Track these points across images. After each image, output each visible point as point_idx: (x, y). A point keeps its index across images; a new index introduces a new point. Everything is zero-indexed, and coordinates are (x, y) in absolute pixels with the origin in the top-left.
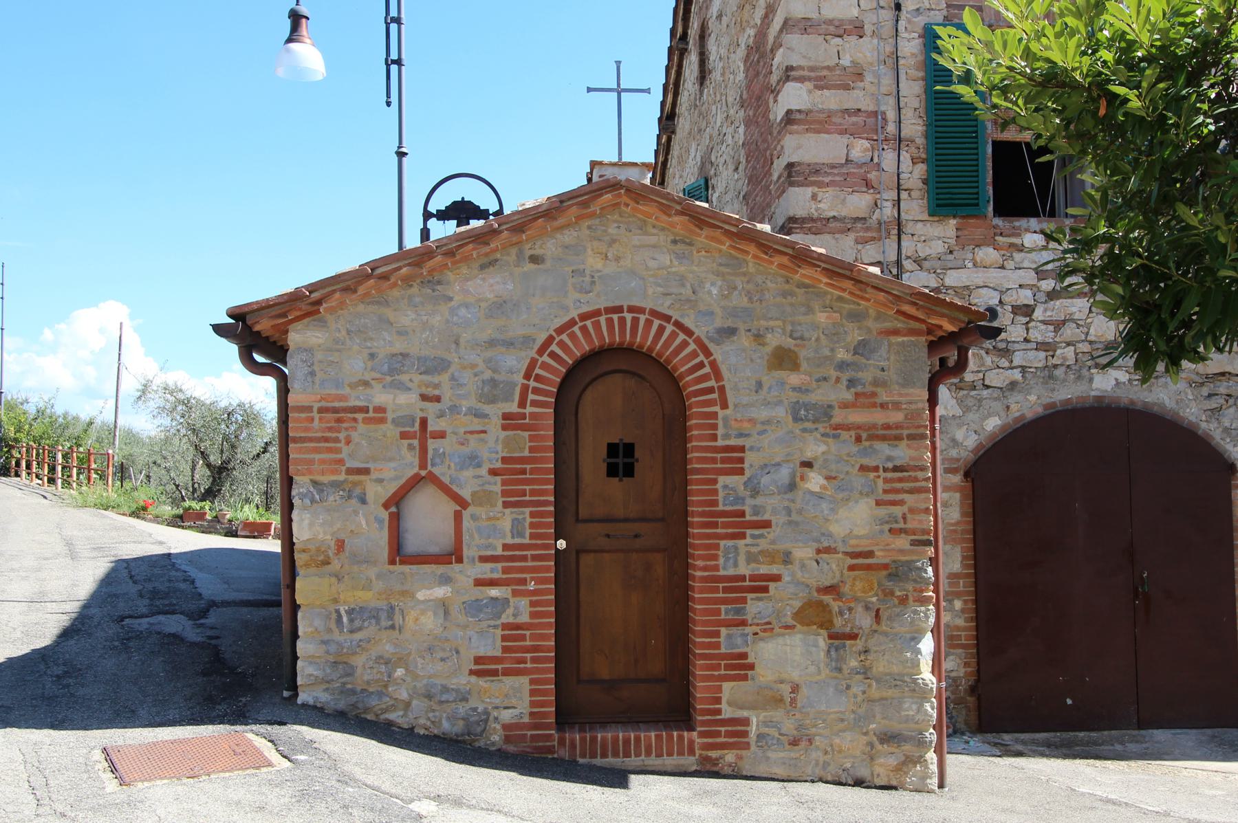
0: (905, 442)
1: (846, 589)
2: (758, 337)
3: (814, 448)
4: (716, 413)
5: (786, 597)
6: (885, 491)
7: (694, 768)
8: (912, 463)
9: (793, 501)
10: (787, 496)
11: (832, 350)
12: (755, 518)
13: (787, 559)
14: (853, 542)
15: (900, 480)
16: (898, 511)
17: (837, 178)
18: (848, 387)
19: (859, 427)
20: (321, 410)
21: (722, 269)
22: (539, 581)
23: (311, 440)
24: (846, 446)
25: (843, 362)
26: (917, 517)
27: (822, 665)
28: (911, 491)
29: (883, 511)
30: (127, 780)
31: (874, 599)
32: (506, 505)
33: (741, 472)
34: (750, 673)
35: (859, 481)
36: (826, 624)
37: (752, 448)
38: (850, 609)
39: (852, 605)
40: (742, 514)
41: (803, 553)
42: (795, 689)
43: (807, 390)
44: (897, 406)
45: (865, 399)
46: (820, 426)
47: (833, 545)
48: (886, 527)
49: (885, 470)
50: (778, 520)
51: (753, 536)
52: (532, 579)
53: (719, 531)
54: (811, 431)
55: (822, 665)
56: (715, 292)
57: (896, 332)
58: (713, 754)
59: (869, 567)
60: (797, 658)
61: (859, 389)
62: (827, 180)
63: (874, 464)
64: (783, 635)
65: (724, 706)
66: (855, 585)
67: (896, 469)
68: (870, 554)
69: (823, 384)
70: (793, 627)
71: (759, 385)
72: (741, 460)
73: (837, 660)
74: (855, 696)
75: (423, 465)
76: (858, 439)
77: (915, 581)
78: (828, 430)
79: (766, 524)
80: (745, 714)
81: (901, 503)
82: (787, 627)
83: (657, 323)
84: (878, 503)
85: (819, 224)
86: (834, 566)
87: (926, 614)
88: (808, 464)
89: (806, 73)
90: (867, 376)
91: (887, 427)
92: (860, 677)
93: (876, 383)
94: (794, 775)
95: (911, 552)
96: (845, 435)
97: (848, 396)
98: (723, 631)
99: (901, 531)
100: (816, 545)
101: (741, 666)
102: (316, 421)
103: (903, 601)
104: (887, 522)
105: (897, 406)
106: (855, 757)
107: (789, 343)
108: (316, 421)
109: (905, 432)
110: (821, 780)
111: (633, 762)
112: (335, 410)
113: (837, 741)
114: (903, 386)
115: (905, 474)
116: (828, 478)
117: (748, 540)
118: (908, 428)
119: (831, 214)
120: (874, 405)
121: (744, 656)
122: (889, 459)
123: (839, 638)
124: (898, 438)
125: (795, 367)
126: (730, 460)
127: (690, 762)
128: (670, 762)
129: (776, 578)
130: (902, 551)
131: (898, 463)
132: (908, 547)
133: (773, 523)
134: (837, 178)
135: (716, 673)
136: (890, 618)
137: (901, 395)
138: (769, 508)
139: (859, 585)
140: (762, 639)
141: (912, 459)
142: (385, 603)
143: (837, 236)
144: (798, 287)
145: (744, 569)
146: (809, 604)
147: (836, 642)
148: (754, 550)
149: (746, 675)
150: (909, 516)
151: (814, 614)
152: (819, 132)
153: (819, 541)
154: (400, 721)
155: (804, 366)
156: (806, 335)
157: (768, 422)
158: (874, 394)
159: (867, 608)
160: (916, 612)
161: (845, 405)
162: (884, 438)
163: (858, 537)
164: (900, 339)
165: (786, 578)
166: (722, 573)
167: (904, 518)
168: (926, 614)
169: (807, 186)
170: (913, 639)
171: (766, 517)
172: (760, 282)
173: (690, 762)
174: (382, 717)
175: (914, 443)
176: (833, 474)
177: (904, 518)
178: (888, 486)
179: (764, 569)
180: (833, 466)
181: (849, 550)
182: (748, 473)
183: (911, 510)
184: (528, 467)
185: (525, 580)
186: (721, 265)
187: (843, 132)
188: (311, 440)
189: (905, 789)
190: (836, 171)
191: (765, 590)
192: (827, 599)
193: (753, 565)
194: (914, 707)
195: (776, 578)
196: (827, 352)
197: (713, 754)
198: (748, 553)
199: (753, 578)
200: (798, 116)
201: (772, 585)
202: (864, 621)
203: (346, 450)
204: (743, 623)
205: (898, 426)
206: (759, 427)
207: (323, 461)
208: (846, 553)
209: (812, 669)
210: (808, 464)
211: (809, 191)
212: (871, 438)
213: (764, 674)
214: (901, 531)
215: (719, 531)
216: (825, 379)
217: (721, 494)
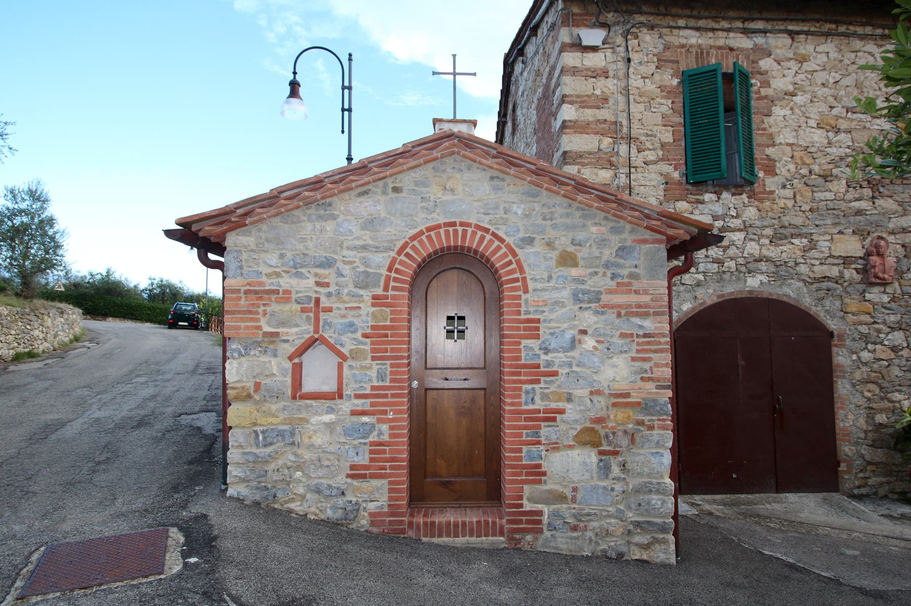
3: (589, 319)
6: (638, 351)
15: (649, 343)
16: (647, 365)
19: (620, 306)
28: (655, 351)
33: (537, 337)
34: (543, 478)
45: (623, 287)
49: (638, 336)
54: (587, 309)
57: (644, 241)
61: (620, 280)
66: (617, 416)
68: (627, 395)
72: (538, 329)
80: (540, 507)
88: (584, 332)
91: (639, 306)
93: (632, 276)
97: (612, 284)
99: (649, 379)
101: (536, 473)
104: (639, 373)
105: (646, 292)
109: (652, 311)
115: (653, 339)
117: (542, 385)
120: (630, 292)
129: (562, 412)
145: (539, 404)
151: (589, 437)
158: (630, 284)
161: (610, 292)
162: (637, 314)
182: (542, 339)
187: (596, 133)
191: (554, 419)
195: (562, 412)
200: (569, 124)
204: (539, 443)
205: (647, 306)
210: (584, 332)
214: (649, 379)
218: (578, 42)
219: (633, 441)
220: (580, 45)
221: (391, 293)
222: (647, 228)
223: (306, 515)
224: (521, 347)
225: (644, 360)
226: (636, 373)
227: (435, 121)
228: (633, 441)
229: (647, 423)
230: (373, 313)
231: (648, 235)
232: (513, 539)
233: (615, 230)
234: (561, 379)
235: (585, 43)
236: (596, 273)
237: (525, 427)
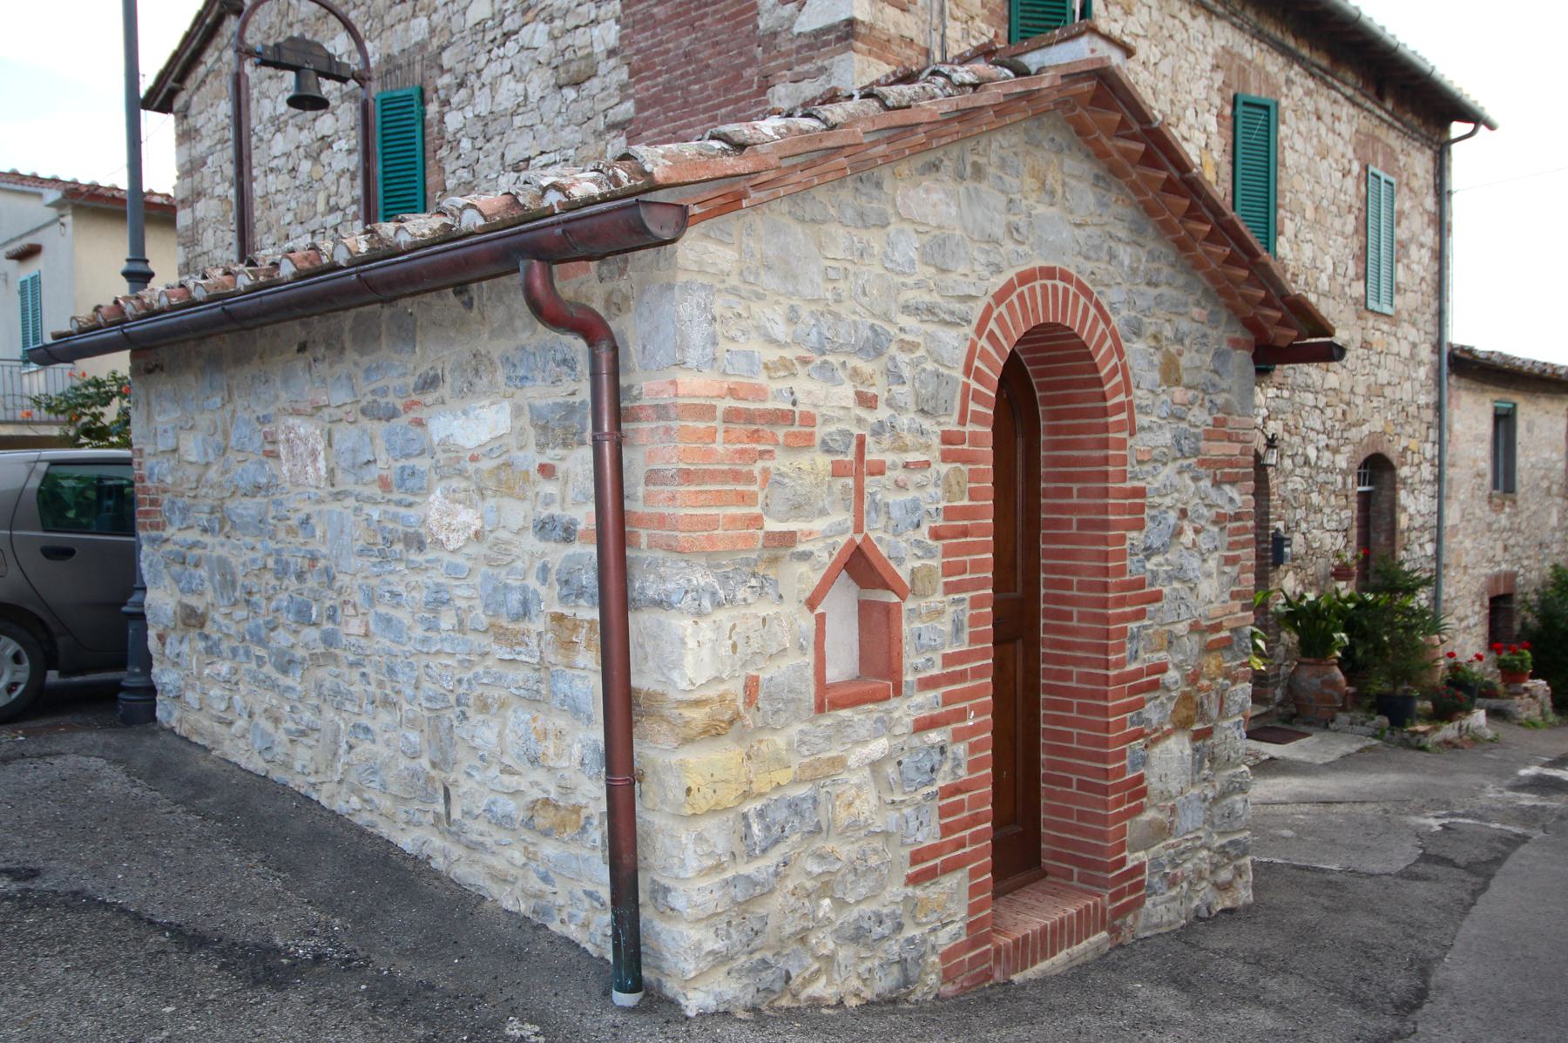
4: (1160, 592)
20: (732, 416)
23: (713, 476)
30: (1446, 943)
52: (972, 707)
75: (858, 528)
102: (720, 437)
108: (720, 437)
112: (750, 417)
149: (946, 519)
174: (803, 995)
188: (713, 476)
207: (733, 520)
221: (970, 428)
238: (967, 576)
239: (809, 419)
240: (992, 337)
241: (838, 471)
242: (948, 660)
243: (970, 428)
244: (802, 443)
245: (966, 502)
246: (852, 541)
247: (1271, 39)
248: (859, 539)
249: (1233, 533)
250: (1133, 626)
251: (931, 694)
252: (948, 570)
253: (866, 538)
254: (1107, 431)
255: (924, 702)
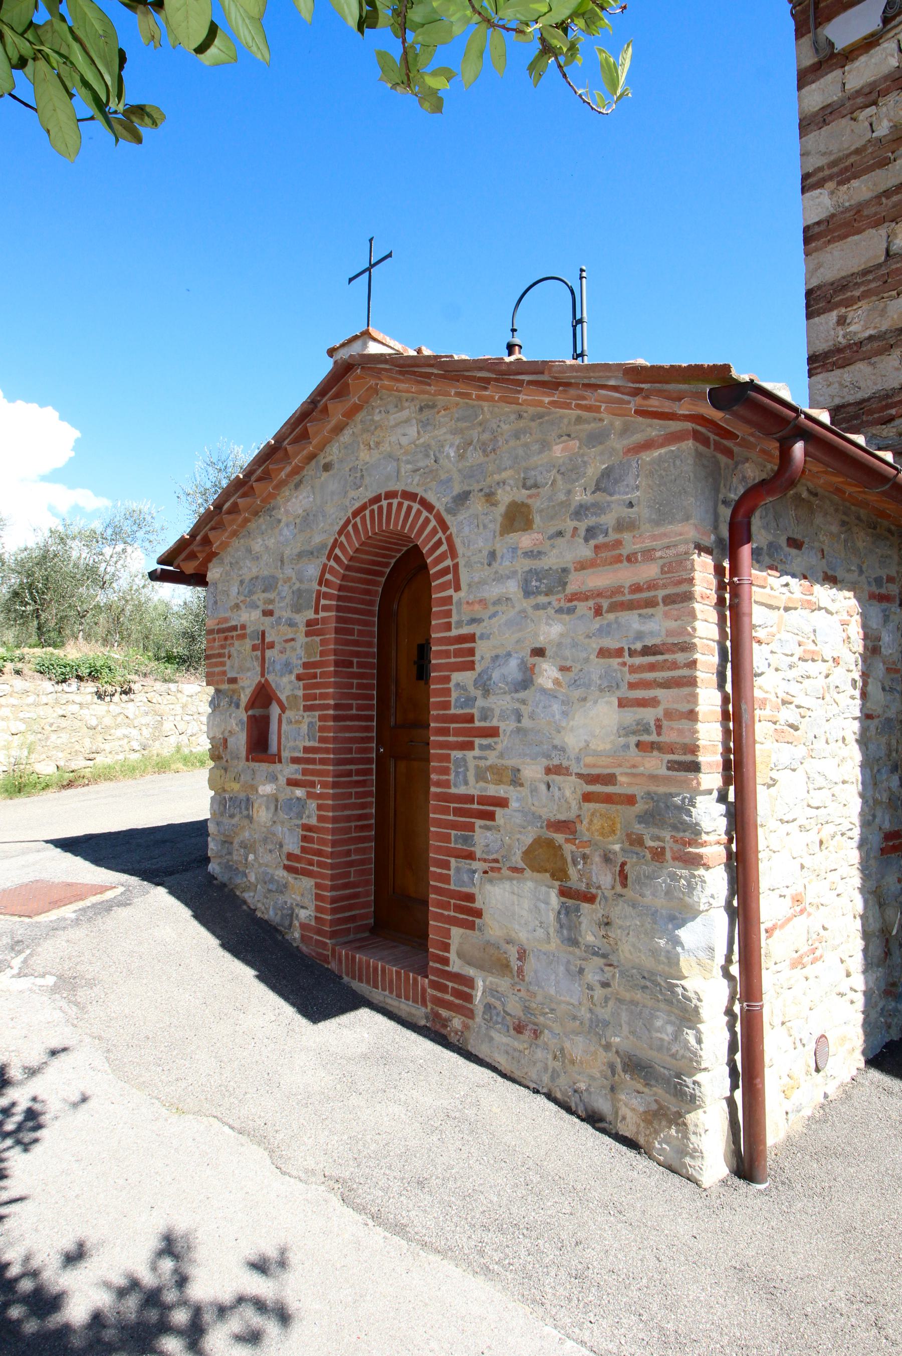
0: (661, 608)
1: (582, 828)
2: (490, 497)
3: (551, 631)
5: (510, 833)
6: (632, 686)
7: (423, 1022)
8: (670, 640)
9: (524, 702)
10: (517, 696)
11: (569, 492)
12: (483, 724)
13: (516, 780)
14: (589, 760)
15: (652, 667)
16: (649, 715)
17: (873, 285)
18: (586, 540)
19: (600, 594)
21: (461, 425)
22: (324, 785)
24: (583, 619)
25: (581, 506)
26: (676, 725)
27: (551, 931)
28: (667, 684)
29: (632, 715)
31: (617, 847)
32: (307, 708)
33: (471, 666)
34: (477, 921)
35: (597, 668)
36: (559, 874)
37: (481, 638)
38: (585, 857)
39: (587, 851)
40: (470, 719)
41: (532, 771)
42: (522, 955)
43: (539, 553)
44: (648, 555)
45: (609, 553)
46: (552, 599)
47: (565, 763)
48: (633, 740)
49: (632, 653)
50: (507, 726)
51: (482, 748)
52: (319, 782)
53: (451, 739)
54: (544, 607)
55: (551, 931)
56: (452, 454)
57: (648, 445)
58: (444, 1013)
59: (608, 799)
60: (524, 913)
61: (601, 539)
62: (857, 293)
63: (617, 645)
64: (511, 879)
65: (452, 956)
66: (592, 820)
67: (647, 651)
68: (610, 779)
69: (560, 540)
70: (522, 871)
71: (493, 555)
72: (472, 652)
73: (570, 929)
74: (590, 988)
76: (598, 612)
77: (675, 828)
78: (562, 604)
79: (493, 732)
80: (471, 972)
81: (653, 702)
82: (515, 869)
83: (406, 503)
84: (622, 703)
85: (848, 353)
86: (568, 793)
87: (689, 883)
88: (539, 652)
89: (827, 172)
90: (608, 519)
91: (636, 588)
92: (600, 961)
93: (622, 526)
94: (517, 1074)
95: (666, 780)
96: (583, 608)
97: (585, 551)
98: (453, 861)
99: (653, 746)
100: (545, 762)
101: (469, 912)
103: (658, 855)
104: (634, 733)
105: (648, 555)
106: (592, 1078)
107: (522, 495)
109: (661, 594)
110: (550, 1097)
111: (377, 995)
113: (567, 1045)
114: (658, 523)
115: (660, 658)
116: (563, 669)
117: (477, 752)
118: (665, 586)
119: (867, 334)
120: (618, 559)
121: (471, 898)
122: (639, 636)
123: (575, 896)
124: (651, 603)
125: (527, 525)
126: (458, 653)
127: (419, 1013)
128: (405, 1007)
129: (502, 803)
130: (653, 778)
131: (649, 642)
132: (663, 771)
133: (501, 731)
134: (873, 285)
135: (446, 913)
136: (638, 880)
137: (654, 538)
138: (497, 712)
139: (597, 823)
140: (491, 881)
141: (669, 633)
142: (245, 794)
143: (874, 360)
144: (533, 420)
145: (473, 788)
146: (538, 842)
147: (570, 902)
148: (482, 763)
150: (665, 723)
151: (546, 857)
152: (846, 237)
153: (548, 757)
154: (249, 901)
155: (537, 519)
156: (540, 479)
157: (498, 602)
158: (618, 543)
159: (607, 859)
160: (674, 877)
161: (582, 566)
162: (630, 606)
163: (596, 754)
164: (656, 454)
165: (514, 804)
166: (453, 790)
167: (659, 727)
168: (689, 883)
169: (831, 310)
170: (672, 918)
171: (495, 723)
172: (495, 427)
173: (419, 1013)
175: (674, 609)
176: (568, 664)
177: (659, 727)
178: (635, 678)
179: (492, 790)
180: (567, 653)
181: (584, 771)
182: (478, 668)
183: (668, 714)
184: (318, 671)
185: (314, 782)
186: (458, 420)
187: (877, 224)
189: (651, 1157)
190: (870, 277)
191: (491, 816)
192: (559, 838)
193: (482, 784)
194: (670, 1029)
195: (502, 803)
196: (562, 497)
197: (444, 1013)
198: (477, 767)
199: (483, 800)
200: (817, 230)
201: (499, 812)
202: (604, 878)
203: (228, 663)
204: (471, 856)
205: (652, 586)
206: (492, 609)
208: (579, 776)
209: (540, 933)
210: (539, 652)
211: (833, 316)
212: (613, 608)
213: (493, 926)
214: (653, 746)
215: (451, 739)
216: (560, 534)
217: (454, 695)
218: (827, 51)
219: (623, 877)
220: (832, 55)
221: (322, 614)
222: (640, 413)
223: (255, 910)
224: (452, 685)
225: (642, 703)
226: (626, 731)
227: (331, 352)
228: (623, 877)
229: (650, 843)
230: (306, 643)
231: (654, 429)
232: (437, 1015)
233: (596, 439)
234: (502, 742)
235: (840, 44)
236: (560, 534)
237: (454, 826)
238: (317, 702)
239: (243, 627)
240: (337, 559)
241: (254, 648)
242: (306, 750)
243: (322, 614)
244: (242, 637)
245: (318, 659)
246: (260, 682)
247: (871, 272)
248: (263, 680)
249: (633, 669)
250: (456, 754)
251: (296, 766)
252: (306, 697)
253: (266, 680)
254: (338, 606)
255: (291, 770)
